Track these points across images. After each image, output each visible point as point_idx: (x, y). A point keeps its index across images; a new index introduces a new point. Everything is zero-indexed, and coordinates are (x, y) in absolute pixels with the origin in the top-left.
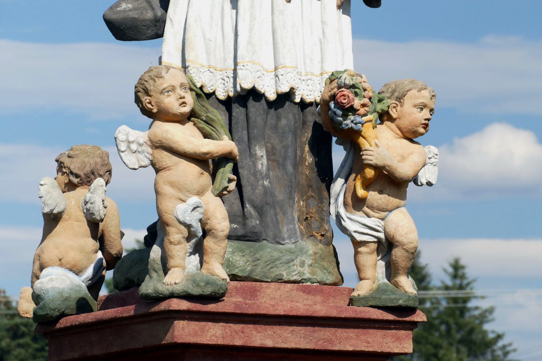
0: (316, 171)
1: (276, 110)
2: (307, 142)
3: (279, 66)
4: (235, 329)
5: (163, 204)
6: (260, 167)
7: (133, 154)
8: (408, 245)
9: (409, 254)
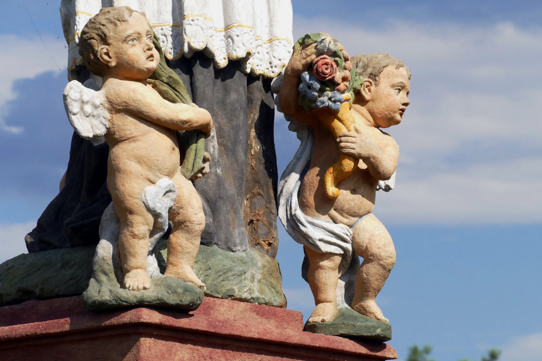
0: (264, 163)
1: (223, 80)
2: (253, 125)
3: (234, 24)
4: (203, 353)
5: (127, 185)
7: (87, 118)
8: (386, 259)
9: (385, 272)
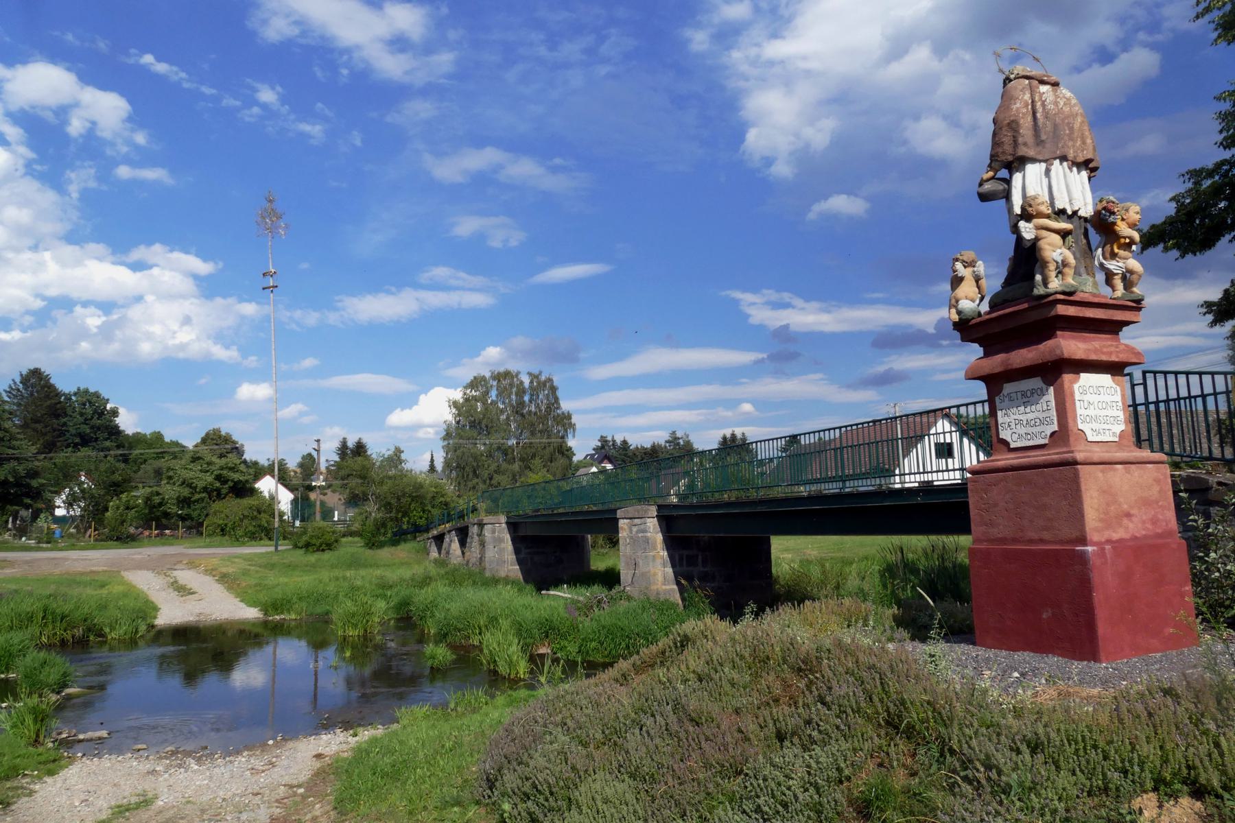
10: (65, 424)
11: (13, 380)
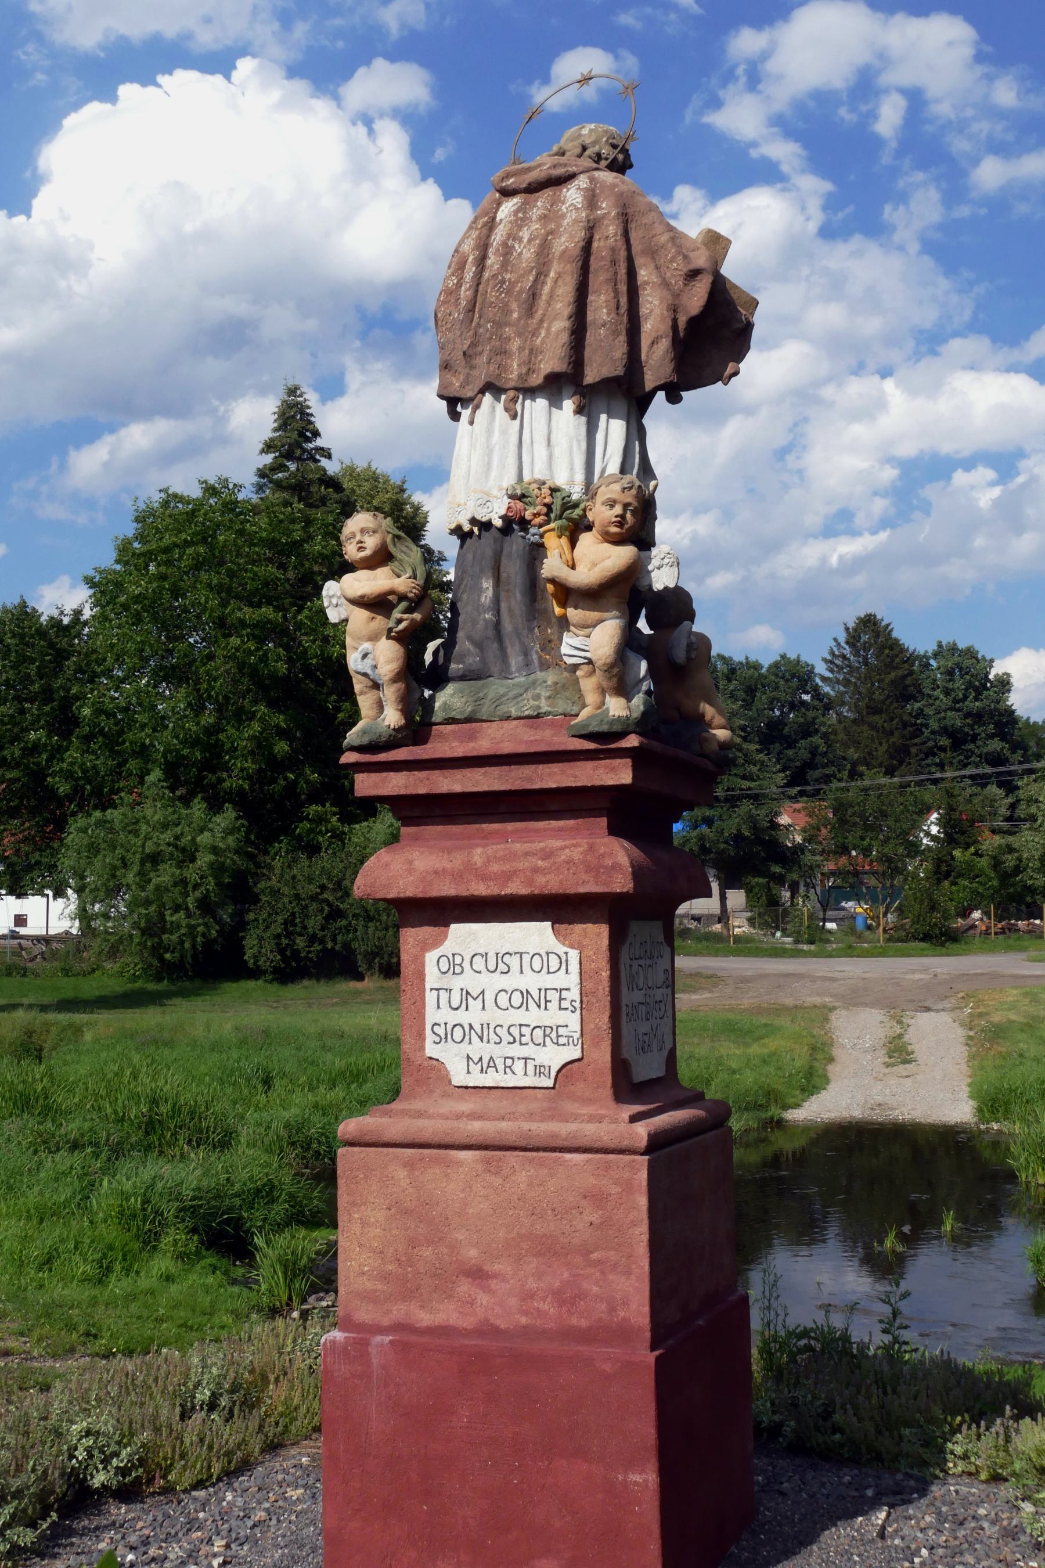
6: (483, 599)
10: (921, 713)
11: (835, 640)
